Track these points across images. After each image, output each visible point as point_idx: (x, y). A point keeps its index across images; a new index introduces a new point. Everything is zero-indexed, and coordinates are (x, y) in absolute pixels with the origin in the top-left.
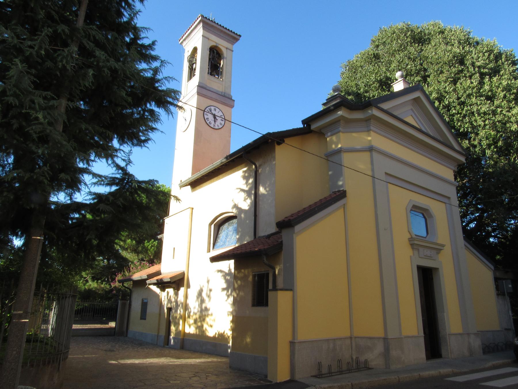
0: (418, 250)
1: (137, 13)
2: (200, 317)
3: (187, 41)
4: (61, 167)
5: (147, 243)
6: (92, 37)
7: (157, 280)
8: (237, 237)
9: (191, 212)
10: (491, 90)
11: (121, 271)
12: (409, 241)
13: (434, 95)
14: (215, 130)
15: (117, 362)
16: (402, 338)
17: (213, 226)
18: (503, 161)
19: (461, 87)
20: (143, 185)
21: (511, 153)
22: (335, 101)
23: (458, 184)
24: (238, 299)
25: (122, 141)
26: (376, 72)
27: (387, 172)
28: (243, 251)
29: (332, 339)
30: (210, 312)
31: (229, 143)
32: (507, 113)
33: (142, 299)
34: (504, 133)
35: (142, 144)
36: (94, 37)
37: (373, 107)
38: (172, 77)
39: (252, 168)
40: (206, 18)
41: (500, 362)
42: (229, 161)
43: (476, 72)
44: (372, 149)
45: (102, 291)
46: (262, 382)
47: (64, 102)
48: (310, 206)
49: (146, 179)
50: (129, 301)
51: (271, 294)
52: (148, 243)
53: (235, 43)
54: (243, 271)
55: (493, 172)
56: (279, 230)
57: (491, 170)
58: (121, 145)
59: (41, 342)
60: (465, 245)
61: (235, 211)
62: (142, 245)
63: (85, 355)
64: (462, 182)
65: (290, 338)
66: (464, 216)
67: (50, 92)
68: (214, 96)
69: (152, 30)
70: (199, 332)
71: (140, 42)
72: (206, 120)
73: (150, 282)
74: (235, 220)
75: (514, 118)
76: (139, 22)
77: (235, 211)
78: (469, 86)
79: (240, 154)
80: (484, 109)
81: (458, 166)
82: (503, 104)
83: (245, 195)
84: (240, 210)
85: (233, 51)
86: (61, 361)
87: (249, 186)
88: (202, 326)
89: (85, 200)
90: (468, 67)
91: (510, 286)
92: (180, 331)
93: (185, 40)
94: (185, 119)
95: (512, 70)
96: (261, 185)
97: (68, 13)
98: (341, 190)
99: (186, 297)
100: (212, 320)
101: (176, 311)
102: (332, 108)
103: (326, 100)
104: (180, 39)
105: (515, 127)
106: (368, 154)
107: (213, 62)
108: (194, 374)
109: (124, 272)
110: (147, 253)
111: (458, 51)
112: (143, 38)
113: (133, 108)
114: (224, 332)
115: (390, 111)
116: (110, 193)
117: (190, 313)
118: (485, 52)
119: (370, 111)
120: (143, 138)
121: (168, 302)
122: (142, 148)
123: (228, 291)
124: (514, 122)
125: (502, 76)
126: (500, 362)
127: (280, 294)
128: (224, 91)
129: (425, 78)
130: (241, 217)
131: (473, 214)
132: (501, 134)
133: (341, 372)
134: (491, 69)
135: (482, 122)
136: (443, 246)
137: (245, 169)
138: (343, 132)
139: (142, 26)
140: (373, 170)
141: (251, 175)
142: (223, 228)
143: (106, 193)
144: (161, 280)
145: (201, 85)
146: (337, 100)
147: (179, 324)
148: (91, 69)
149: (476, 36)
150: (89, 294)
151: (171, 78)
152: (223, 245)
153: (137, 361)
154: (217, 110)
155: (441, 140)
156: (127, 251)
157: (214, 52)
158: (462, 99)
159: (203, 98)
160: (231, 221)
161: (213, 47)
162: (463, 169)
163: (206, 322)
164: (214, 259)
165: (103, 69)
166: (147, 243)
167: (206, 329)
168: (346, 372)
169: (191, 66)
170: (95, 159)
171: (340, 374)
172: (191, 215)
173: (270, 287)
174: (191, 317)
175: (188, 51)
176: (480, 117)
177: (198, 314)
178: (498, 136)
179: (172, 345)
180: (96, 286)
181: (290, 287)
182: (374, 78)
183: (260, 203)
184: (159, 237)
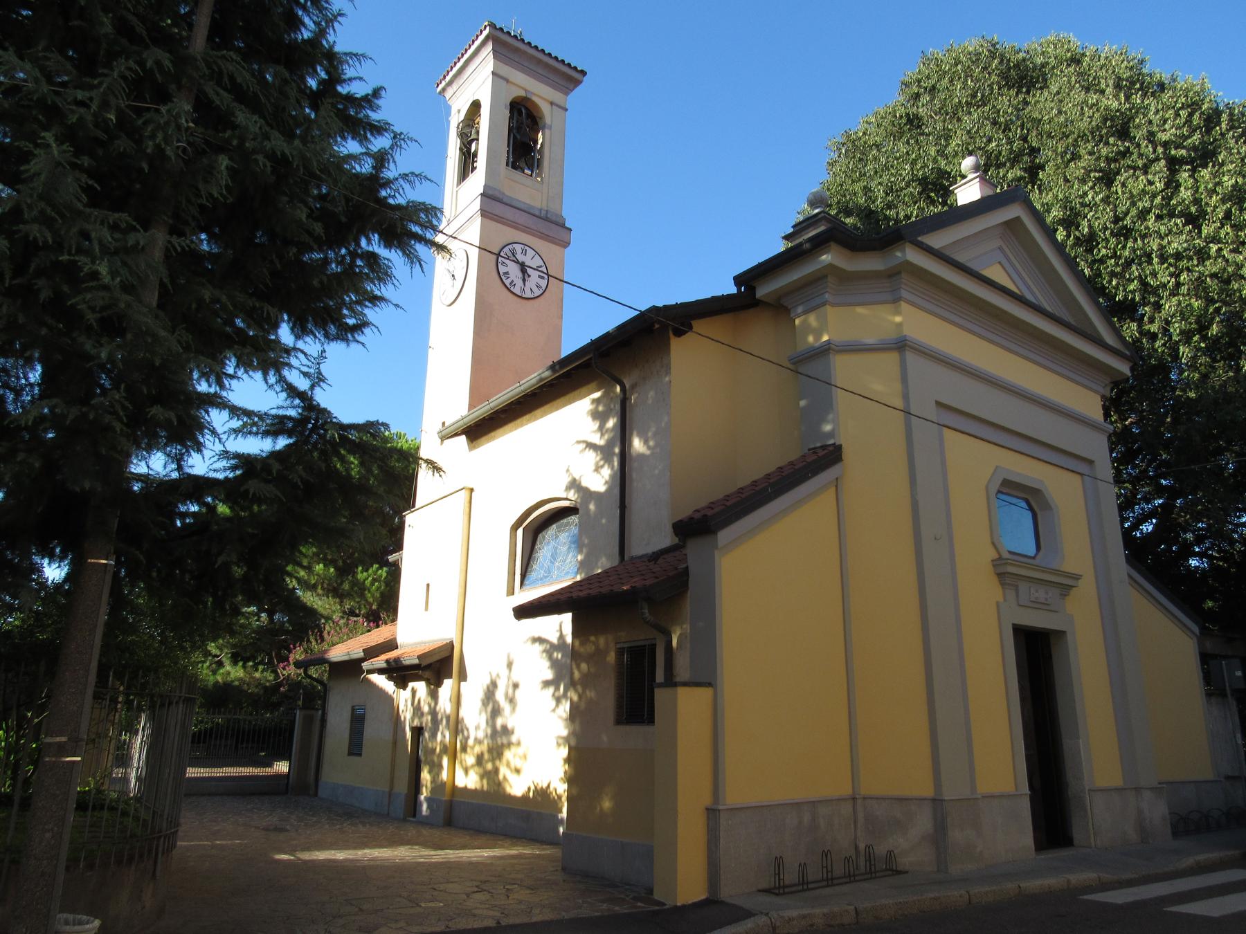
0: (1016, 588)
2: (490, 750)
3: (455, 86)
4: (154, 392)
6: (226, 79)
7: (387, 661)
8: (580, 558)
10: (1196, 201)
11: (302, 641)
12: (994, 566)
13: (1056, 213)
15: (292, 858)
16: (977, 799)
17: (520, 532)
19: (1123, 193)
20: (353, 436)
23: (1112, 427)
24: (583, 706)
25: (300, 330)
30: (514, 739)
34: (1225, 303)
35: (349, 335)
36: (232, 78)
37: (908, 244)
38: (420, 175)
39: (614, 392)
40: (501, 29)
41: (1214, 855)
45: (257, 687)
46: (639, 904)
47: (160, 237)
48: (755, 483)
49: (360, 419)
50: (320, 712)
51: (660, 695)
52: (365, 574)
57: (1192, 395)
58: (298, 337)
59: (112, 809)
60: (1130, 577)
61: (572, 495)
62: (350, 578)
65: (707, 800)
66: (1126, 504)
68: (522, 218)
72: (503, 277)
73: (371, 667)
76: (341, 39)
77: (572, 495)
78: (1143, 190)
80: (1176, 245)
81: (1112, 385)
82: (1222, 233)
83: (598, 458)
84: (585, 493)
85: (566, 110)
87: (606, 437)
88: (496, 771)
89: (214, 470)
91: (1239, 673)
92: (443, 784)
93: (450, 83)
94: (453, 276)
97: (169, 21)
99: (457, 701)
100: (520, 758)
102: (807, 246)
103: (793, 227)
107: (518, 137)
109: (309, 641)
110: (362, 596)
112: (350, 79)
114: (549, 786)
115: (948, 253)
116: (274, 455)
117: (467, 738)
119: (899, 254)
120: (351, 321)
123: (557, 689)
125: (1222, 165)
126: (1214, 855)
129: (1033, 171)
130: (588, 509)
132: (1217, 305)
133: (830, 881)
136: (1077, 577)
137: (597, 395)
140: (906, 397)
142: (544, 537)
143: (264, 455)
144: (397, 660)
145: (490, 192)
147: (440, 767)
148: (223, 156)
149: (1157, 70)
151: (417, 176)
152: (546, 577)
153: (340, 855)
154: (530, 252)
155: (1073, 322)
157: (520, 113)
158: (1128, 221)
160: (565, 521)
164: (523, 612)
165: (254, 157)
166: (362, 572)
167: (505, 778)
169: (465, 146)
171: (828, 886)
172: (467, 505)
173: (660, 677)
174: (469, 750)
175: (459, 111)
177: (486, 742)
178: (1211, 310)
181: (706, 679)
182: (909, 173)
183: (634, 475)
184: (392, 558)
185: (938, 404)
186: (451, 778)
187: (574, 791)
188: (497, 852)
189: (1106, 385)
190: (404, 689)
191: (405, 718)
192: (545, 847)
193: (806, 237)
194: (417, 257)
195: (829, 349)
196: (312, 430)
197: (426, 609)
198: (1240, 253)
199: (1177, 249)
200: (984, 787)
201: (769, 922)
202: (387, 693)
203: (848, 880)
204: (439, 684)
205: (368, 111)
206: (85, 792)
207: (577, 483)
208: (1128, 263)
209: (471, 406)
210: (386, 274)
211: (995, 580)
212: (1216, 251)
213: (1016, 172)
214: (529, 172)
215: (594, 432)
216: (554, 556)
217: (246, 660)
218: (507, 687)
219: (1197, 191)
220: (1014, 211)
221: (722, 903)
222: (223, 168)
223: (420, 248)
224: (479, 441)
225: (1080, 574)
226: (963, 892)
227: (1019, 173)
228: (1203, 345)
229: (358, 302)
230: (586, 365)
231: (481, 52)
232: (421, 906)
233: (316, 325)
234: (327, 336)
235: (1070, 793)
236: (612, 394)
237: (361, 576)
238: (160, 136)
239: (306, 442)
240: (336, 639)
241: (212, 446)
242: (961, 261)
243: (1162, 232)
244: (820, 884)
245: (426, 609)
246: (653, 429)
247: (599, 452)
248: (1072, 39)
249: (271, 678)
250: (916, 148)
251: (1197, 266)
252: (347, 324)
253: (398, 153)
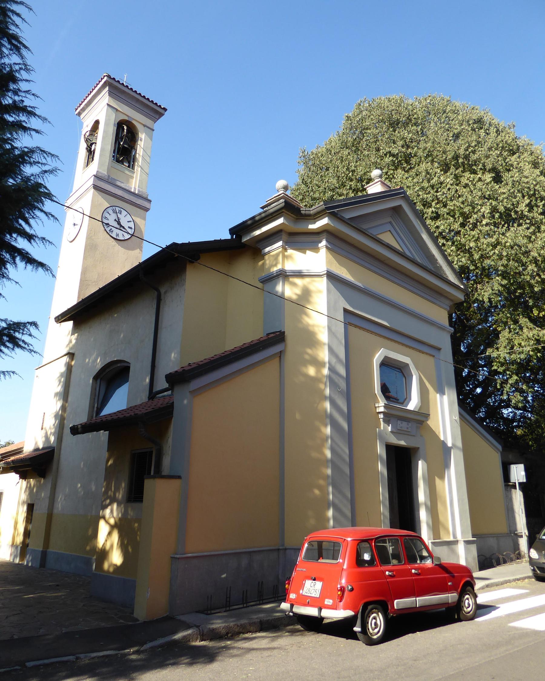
40: (114, 79)
85: (153, 130)
175: (87, 126)
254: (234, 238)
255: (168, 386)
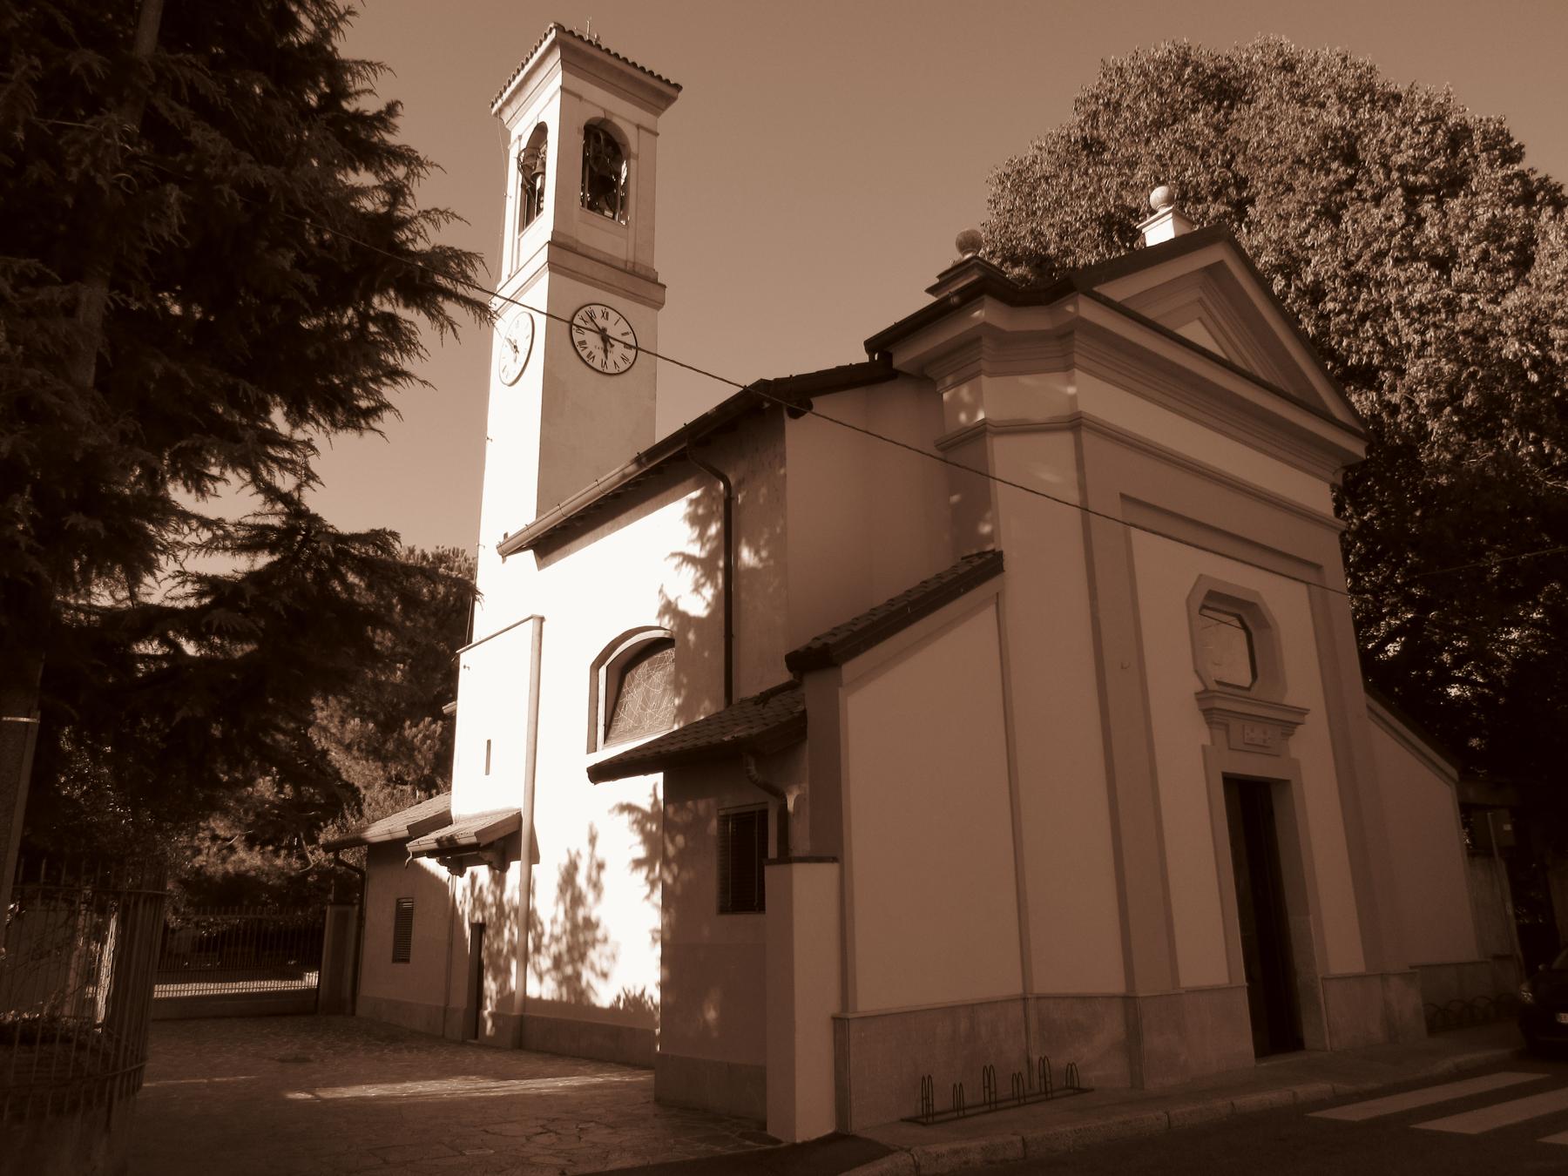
1: (341, 17)
2: (570, 949)
3: (514, 105)
4: (75, 496)
5: (410, 728)
6: (185, 91)
7: (438, 841)
8: (677, 701)
9: (538, 629)
10: (1445, 239)
11: (335, 817)
12: (1198, 700)
13: (1266, 259)
14: (608, 378)
15: (310, 1096)
16: (1180, 994)
17: (603, 671)
18: (1481, 454)
19: (1355, 231)
20: (356, 550)
21: (1502, 426)
22: (965, 279)
23: (1344, 523)
24: (678, 890)
25: (298, 415)
26: (1091, 193)
27: (1126, 492)
28: (686, 745)
29: (967, 1006)
30: (599, 934)
31: (650, 415)
32: (1489, 308)
33: (398, 900)
34: (1481, 366)
35: (363, 422)
36: (192, 89)
37: (1081, 296)
38: (446, 211)
39: (717, 490)
40: (571, 33)
41: (1466, 1058)
42: (645, 469)
43: (1393, 183)
44: (1080, 425)
45: (279, 878)
46: (748, 1143)
47: (94, 297)
48: (891, 602)
49: (362, 528)
50: (357, 908)
51: (772, 874)
52: (414, 730)
53: (663, 110)
54: (690, 804)
55: (1451, 486)
56: (794, 677)
57: (1443, 480)
58: (295, 425)
59: (66, 1040)
60: (1370, 708)
61: (667, 622)
62: (395, 735)
63: (216, 1077)
64: (1359, 519)
65: (833, 1007)
66: (1364, 622)
67: (36, 260)
68: (601, 273)
69: (389, 69)
70: (568, 993)
71: (349, 106)
72: (578, 348)
73: (417, 849)
74: (669, 651)
75: (1511, 321)
76: (346, 46)
77: (667, 622)
78: (1379, 228)
79: (676, 450)
80: (1420, 295)
81: (1344, 471)
82: (1477, 279)
83: (698, 574)
84: (683, 619)
86: (115, 1100)
87: (708, 547)
88: (578, 976)
89: (172, 599)
90: (1368, 172)
91: (1508, 827)
92: (512, 994)
93: (508, 102)
94: (515, 347)
95: (1503, 178)
96: (743, 541)
97: (110, 16)
98: (989, 552)
99: (528, 889)
100: (607, 958)
101: (499, 932)
102: (955, 300)
103: (939, 277)
104: (494, 100)
105: (1513, 349)
106: (1067, 438)
107: (596, 169)
108: (542, 1126)
109: (343, 817)
110: (411, 758)
111: (1337, 121)
112: (358, 93)
113: (329, 310)
114: (643, 993)
115: (1133, 307)
116: (253, 577)
117: (540, 936)
118: (1420, 124)
119: (1070, 309)
120: (364, 404)
121: (474, 904)
122: (361, 434)
123: (652, 869)
124: (1510, 333)
125: (1475, 194)
126: (1466, 1058)
127: (800, 872)
128: (631, 258)
129: (1240, 208)
130: (687, 641)
131: (1393, 614)
132: (1471, 369)
133: (993, 1105)
134: (1440, 174)
135: (1415, 336)
136: (1303, 712)
137: (695, 494)
138: (991, 375)
139: (359, 57)
140: (1082, 488)
141: (713, 513)
142: (633, 677)
143: (239, 576)
144: (451, 839)
145: (561, 240)
146: (971, 276)
147: (508, 971)
148: (172, 185)
149: (1392, 78)
150: (238, 889)
151: (441, 213)
152: (636, 728)
153: (372, 1091)
154: (613, 316)
155: (1292, 392)
156: (350, 753)
157: (597, 138)
158: (1359, 267)
159: (568, 280)
160: (659, 655)
161: (595, 124)
162: (1361, 479)
163: (587, 963)
164: (600, 773)
165: (216, 187)
166: (410, 728)
167: (588, 983)
168: (1010, 1103)
169: (529, 182)
170: (222, 473)
171: (990, 1111)
172: (537, 638)
173: (772, 852)
174: (543, 950)
175: (520, 137)
176: (1408, 321)
177: (564, 940)
178: (1464, 375)
179: (490, 1037)
180: (259, 863)
181: (830, 851)
182: (1086, 211)
183: (743, 595)
184: (446, 709)
185: (1123, 496)
186: (521, 986)
187: (670, 1000)
188: (575, 1081)
189: (1336, 471)
190: (461, 876)
191: (463, 912)
192: (637, 1072)
193: (953, 290)
194: (447, 319)
195: (986, 430)
196: (303, 544)
197: (487, 773)
198: (1499, 304)
199: (1421, 300)
200: (1188, 980)
201: (912, 1161)
202: (441, 880)
203: (1016, 1102)
204: (504, 867)
205: (383, 133)
206: (35, 1020)
207: (673, 606)
208: (1363, 317)
209: (539, 512)
210: (410, 342)
211: (1200, 718)
212: (1469, 301)
213: (1217, 208)
214: (611, 214)
215: (693, 541)
216: (645, 703)
217: (263, 845)
218: (590, 868)
219: (1445, 226)
220: (1216, 254)
221: (854, 1138)
222: (172, 200)
223: (450, 308)
224: (550, 556)
225: (1307, 707)
226: (1160, 1113)
227: (1222, 209)
228: (1456, 419)
229: (376, 380)
230: (680, 457)
231: (544, 66)
232: (465, 1155)
233: (319, 410)
234: (334, 424)
235: (1298, 980)
236: (714, 494)
237: (408, 733)
238: (87, 160)
239: (296, 559)
240: (378, 813)
241: (167, 565)
242: (1151, 318)
243: (1402, 279)
244: (981, 1109)
245: (487, 773)
246: (766, 536)
247: (699, 567)
248: (1285, 40)
249: (297, 865)
250: (1096, 179)
251: (1446, 320)
252: (359, 407)
253: (416, 184)
254: (876, 358)
255: (792, 678)
